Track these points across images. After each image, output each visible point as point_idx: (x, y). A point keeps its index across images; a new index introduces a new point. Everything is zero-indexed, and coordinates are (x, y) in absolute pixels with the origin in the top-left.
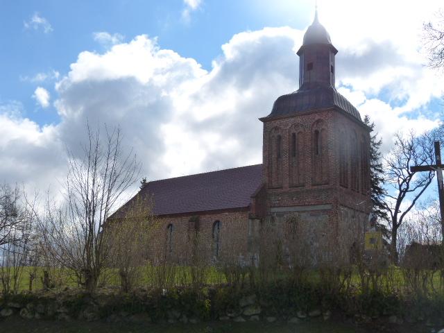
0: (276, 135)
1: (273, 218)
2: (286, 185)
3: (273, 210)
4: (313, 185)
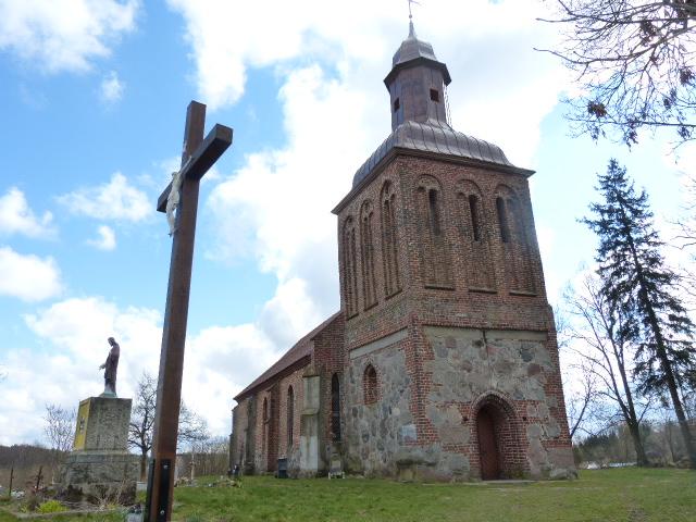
0: (350, 229)
1: (351, 368)
2: (361, 309)
3: (354, 354)
4: (387, 299)
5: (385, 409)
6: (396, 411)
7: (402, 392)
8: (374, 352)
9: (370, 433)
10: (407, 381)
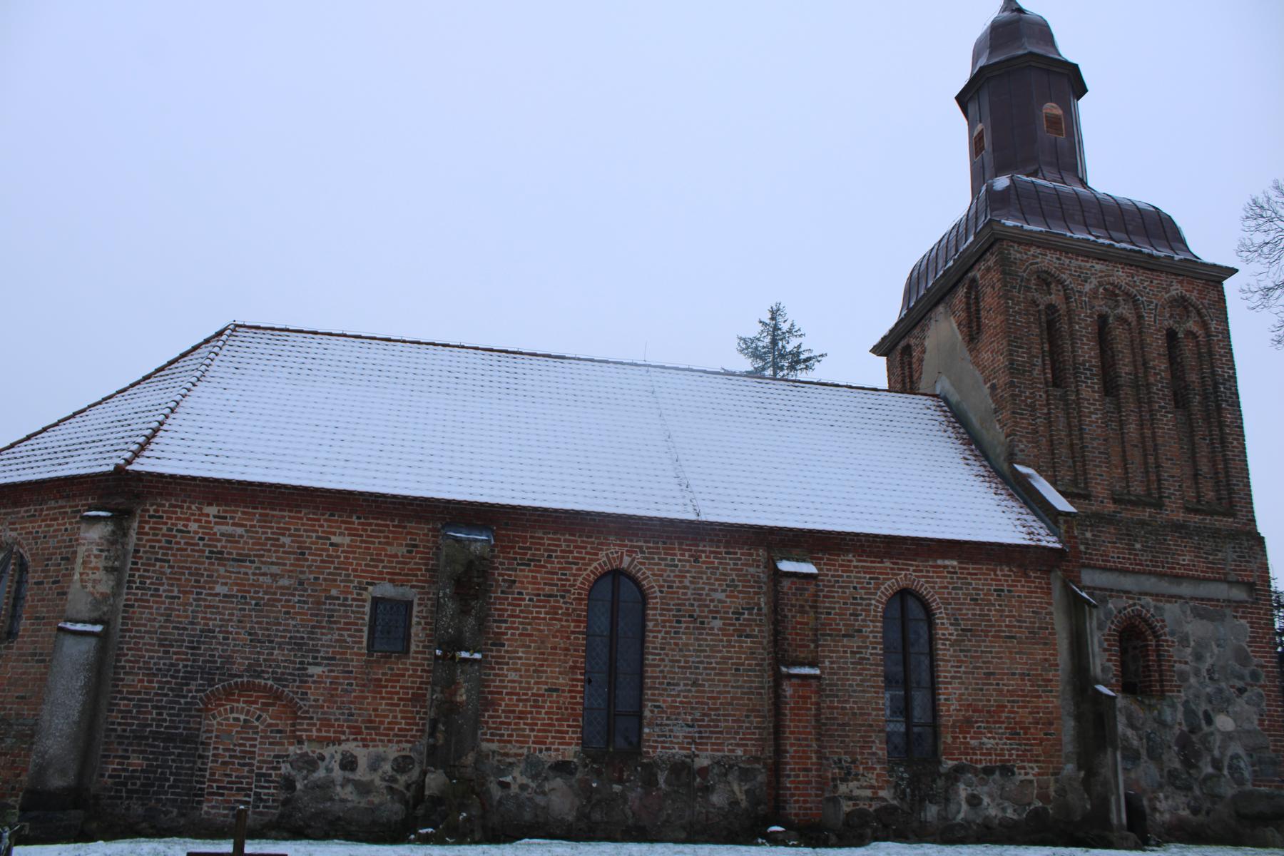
5: (1189, 713)
6: (1224, 722)
7: (1241, 691)
8: (1157, 596)
9: (1143, 752)
10: (1255, 676)
